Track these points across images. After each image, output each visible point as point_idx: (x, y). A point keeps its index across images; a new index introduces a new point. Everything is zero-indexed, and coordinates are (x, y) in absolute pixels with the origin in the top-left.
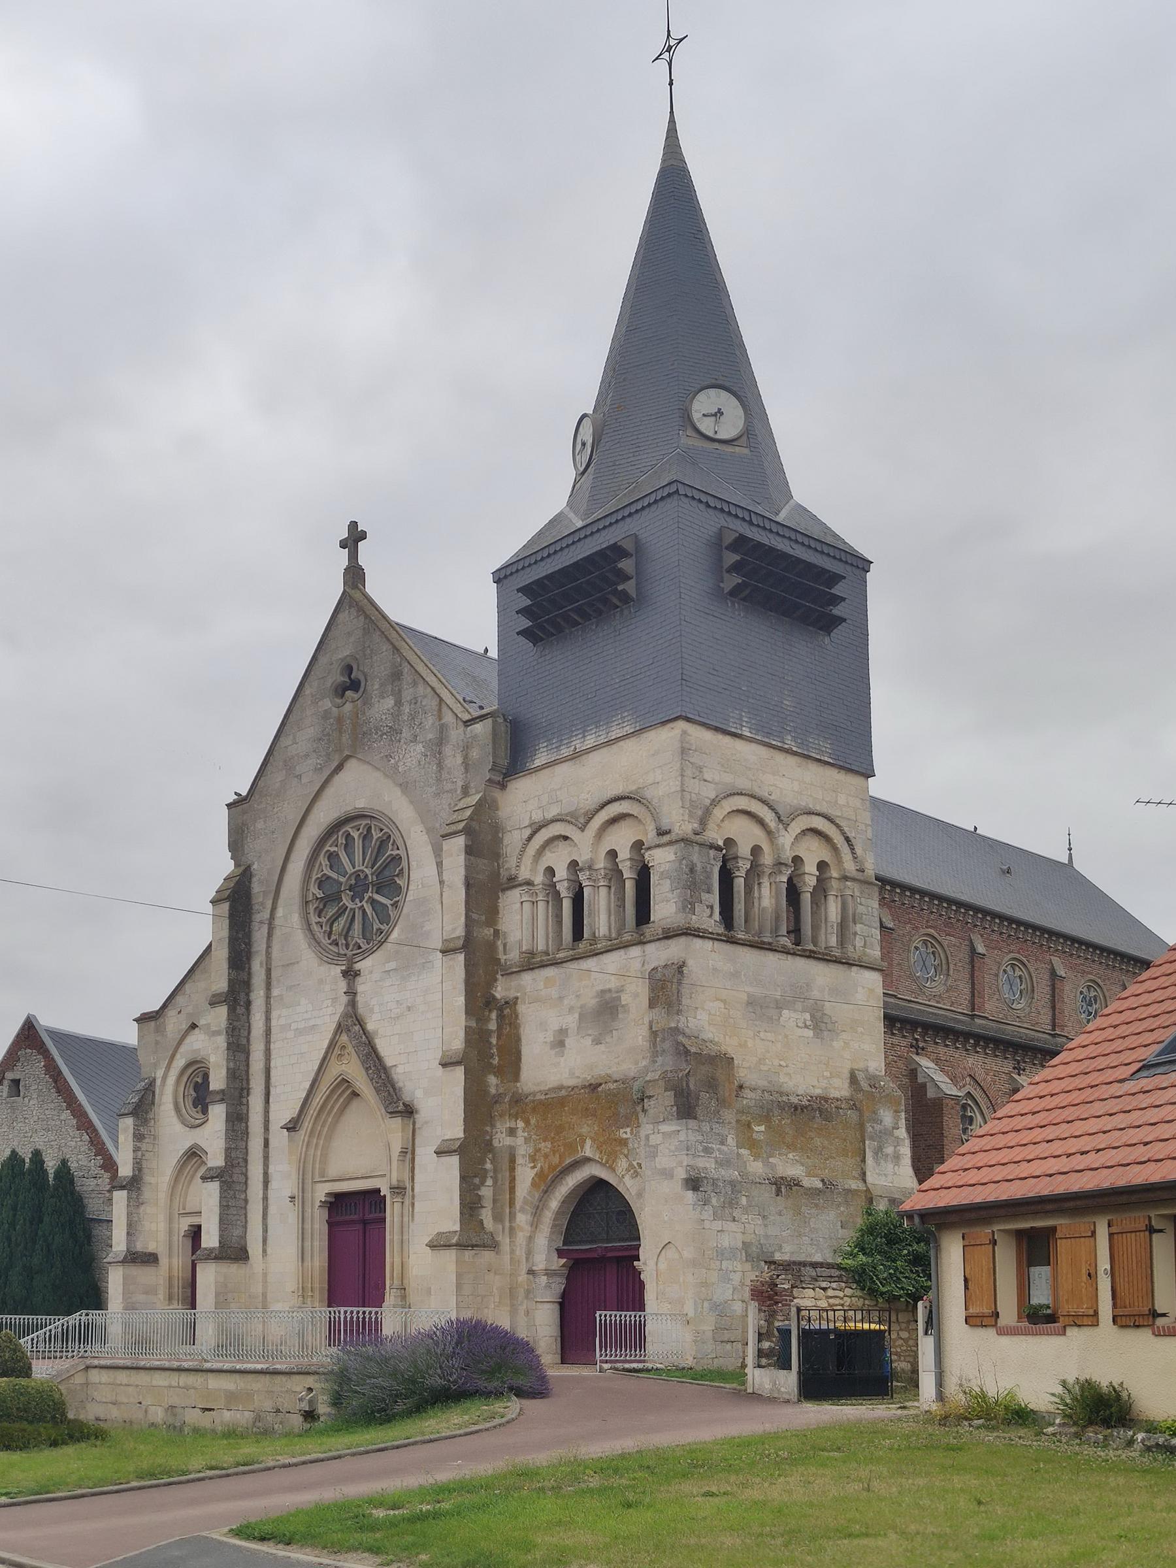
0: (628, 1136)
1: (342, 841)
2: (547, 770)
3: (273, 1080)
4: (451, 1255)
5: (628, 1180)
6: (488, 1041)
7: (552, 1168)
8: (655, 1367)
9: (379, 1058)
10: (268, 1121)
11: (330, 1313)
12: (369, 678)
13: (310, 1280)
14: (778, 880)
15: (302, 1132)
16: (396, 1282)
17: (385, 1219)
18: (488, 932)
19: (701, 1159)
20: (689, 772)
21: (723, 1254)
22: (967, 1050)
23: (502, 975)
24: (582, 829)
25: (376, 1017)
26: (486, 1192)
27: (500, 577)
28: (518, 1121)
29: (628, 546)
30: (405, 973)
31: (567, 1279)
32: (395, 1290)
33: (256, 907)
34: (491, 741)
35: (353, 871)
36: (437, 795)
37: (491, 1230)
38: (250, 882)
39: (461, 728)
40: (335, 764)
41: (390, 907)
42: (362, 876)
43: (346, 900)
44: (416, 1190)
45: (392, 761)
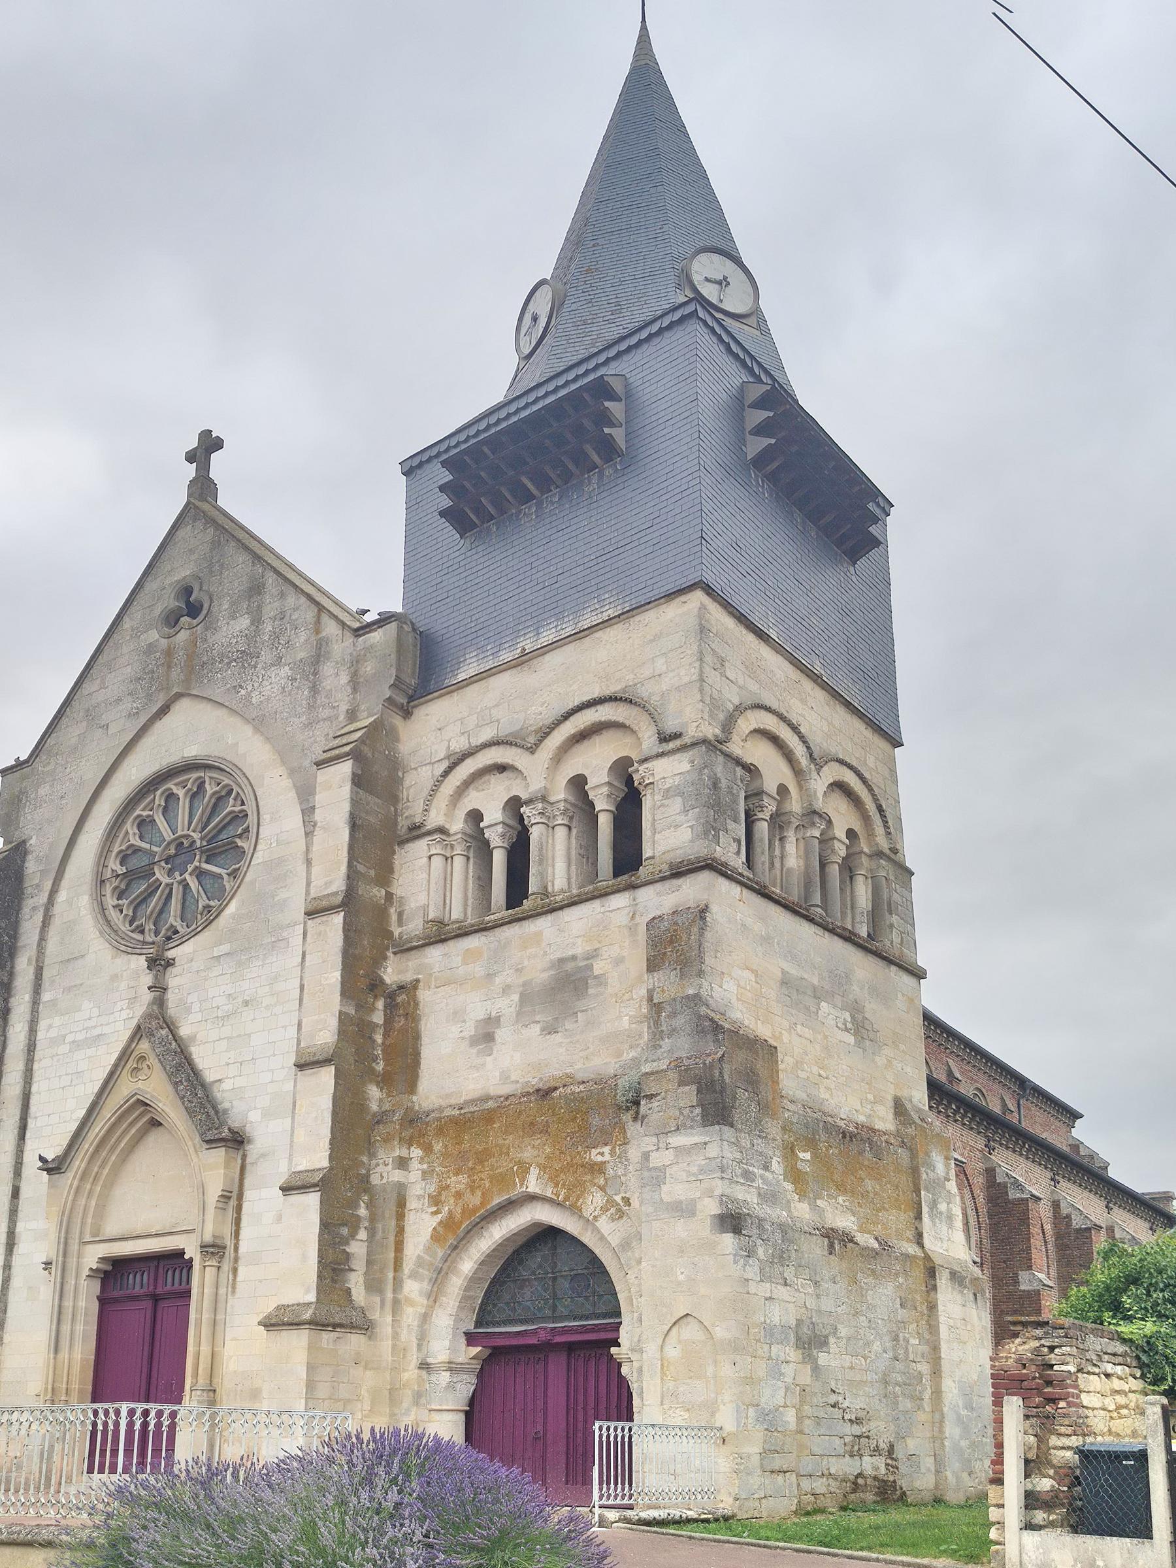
0: (607, 1157)
1: (160, 801)
2: (475, 684)
3: (33, 1109)
4: (298, 1342)
5: (604, 1224)
6: (370, 1038)
7: (467, 1212)
8: (684, 1516)
9: (196, 1073)
10: (21, 1164)
11: (96, 1413)
12: (215, 598)
13: (65, 1379)
14: (808, 834)
15: (70, 1175)
16: (202, 1381)
17: (187, 1294)
18: (379, 893)
19: (739, 1187)
20: (708, 659)
21: (772, 1335)
22: (948, 1116)
23: (395, 953)
24: (532, 750)
25: (195, 1017)
26: (358, 1248)
27: (412, 468)
28: (412, 1149)
29: (617, 386)
30: (243, 957)
31: (481, 1375)
32: (199, 1393)
33: (28, 891)
34: (394, 650)
35: (173, 837)
36: (309, 725)
37: (363, 1304)
38: (23, 861)
39: (349, 639)
40: (159, 705)
41: (225, 877)
42: (186, 843)
43: (160, 875)
44: (243, 1249)
45: (243, 692)
